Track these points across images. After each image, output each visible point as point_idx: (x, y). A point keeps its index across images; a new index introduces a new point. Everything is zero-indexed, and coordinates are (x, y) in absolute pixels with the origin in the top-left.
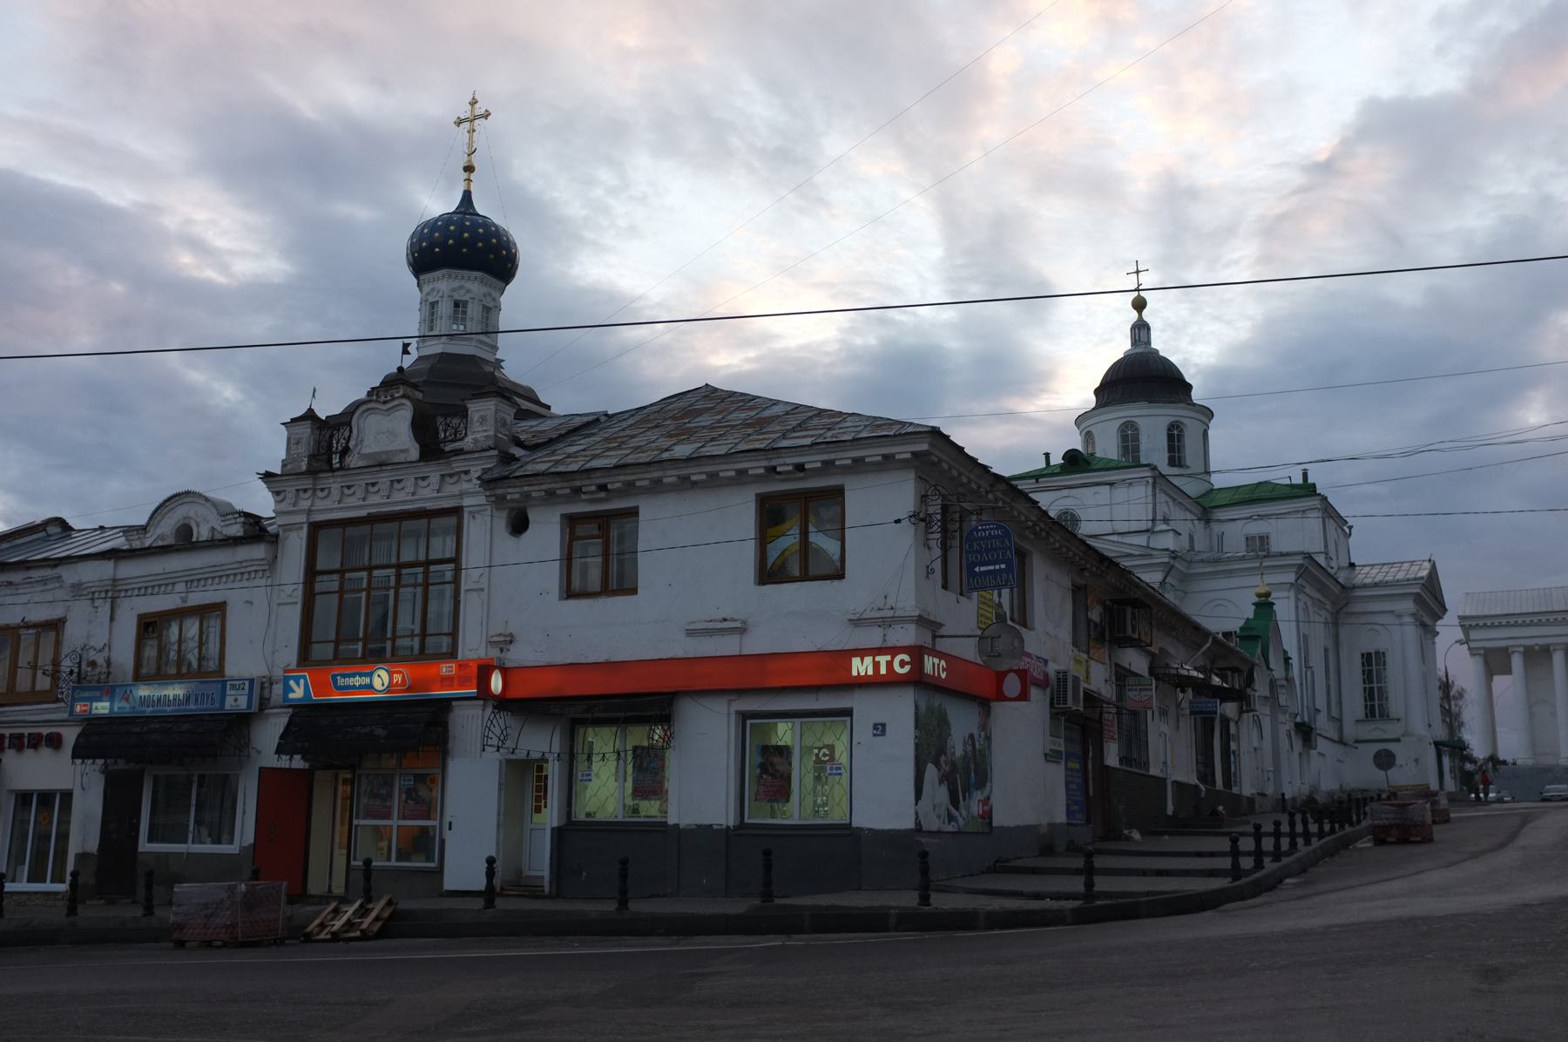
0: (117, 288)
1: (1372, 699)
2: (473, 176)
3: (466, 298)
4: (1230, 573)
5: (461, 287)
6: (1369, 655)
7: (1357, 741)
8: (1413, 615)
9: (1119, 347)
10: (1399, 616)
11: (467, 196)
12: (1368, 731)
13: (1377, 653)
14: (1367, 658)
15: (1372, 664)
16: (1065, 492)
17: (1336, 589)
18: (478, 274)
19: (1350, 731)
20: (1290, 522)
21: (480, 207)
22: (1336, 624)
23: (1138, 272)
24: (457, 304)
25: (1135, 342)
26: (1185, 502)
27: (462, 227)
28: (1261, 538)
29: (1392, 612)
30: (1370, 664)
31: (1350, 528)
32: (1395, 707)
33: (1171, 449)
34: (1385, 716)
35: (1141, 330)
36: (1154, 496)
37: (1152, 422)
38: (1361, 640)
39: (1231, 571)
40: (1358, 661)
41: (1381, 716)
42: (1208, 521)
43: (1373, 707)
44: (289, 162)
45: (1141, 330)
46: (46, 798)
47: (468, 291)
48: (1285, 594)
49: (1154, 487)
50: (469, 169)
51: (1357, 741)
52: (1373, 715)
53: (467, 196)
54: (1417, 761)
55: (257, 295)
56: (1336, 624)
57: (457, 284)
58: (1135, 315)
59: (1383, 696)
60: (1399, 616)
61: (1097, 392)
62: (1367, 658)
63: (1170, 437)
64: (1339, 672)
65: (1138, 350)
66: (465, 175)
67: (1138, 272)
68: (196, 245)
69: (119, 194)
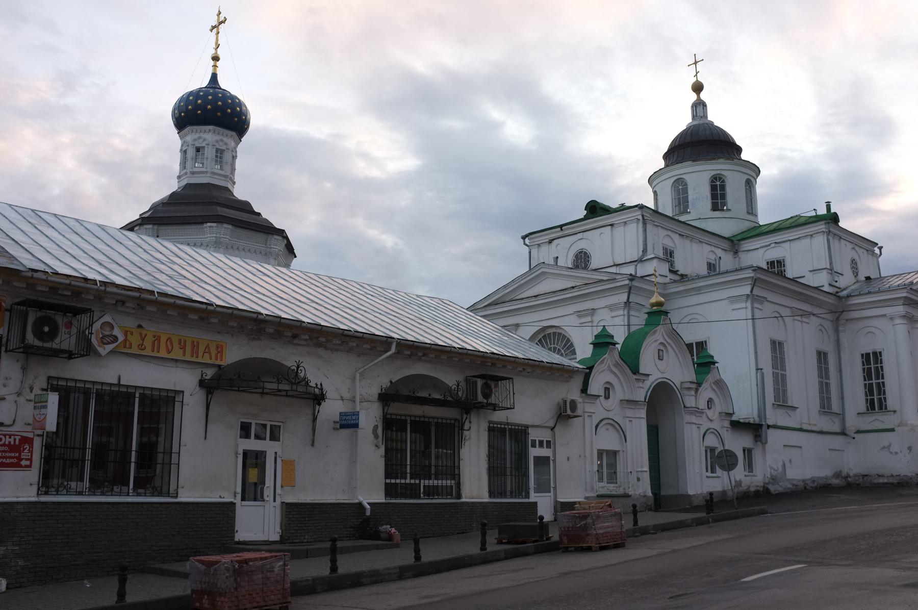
0: (328, 185)
1: (872, 394)
2: (218, 63)
3: (224, 148)
4: (698, 291)
5: (199, 138)
6: (868, 355)
7: (858, 432)
8: (904, 317)
9: (682, 121)
10: (891, 319)
11: (214, 77)
12: (869, 422)
13: (875, 353)
14: (866, 358)
15: (873, 364)
16: (580, 236)
17: (831, 300)
18: (211, 127)
19: (852, 422)
20: (796, 245)
21: (223, 83)
22: (837, 331)
23: (696, 63)
24: (217, 150)
25: (694, 117)
26: (739, 237)
27: (207, 94)
28: (779, 262)
29: (885, 315)
30: (869, 363)
31: (880, 248)
32: (892, 401)
33: (714, 196)
34: (883, 406)
35: (699, 107)
36: (645, 230)
37: (698, 176)
38: (858, 343)
39: (700, 288)
40: (858, 361)
41: (881, 408)
42: (736, 252)
43: (872, 401)
44: (416, 101)
45: (699, 107)
46: (608, 452)
47: (204, 140)
48: (743, 305)
49: (645, 223)
50: (216, 58)
51: (858, 432)
52: (873, 408)
53: (214, 77)
54: (910, 448)
55: (405, 181)
56: (837, 331)
57: (218, 138)
58: (694, 97)
59: (881, 388)
60: (891, 319)
61: (666, 156)
62: (866, 358)
63: (713, 188)
64: (840, 371)
65: (696, 123)
66: (212, 63)
67: (696, 63)
68: (365, 156)
69: (319, 131)
